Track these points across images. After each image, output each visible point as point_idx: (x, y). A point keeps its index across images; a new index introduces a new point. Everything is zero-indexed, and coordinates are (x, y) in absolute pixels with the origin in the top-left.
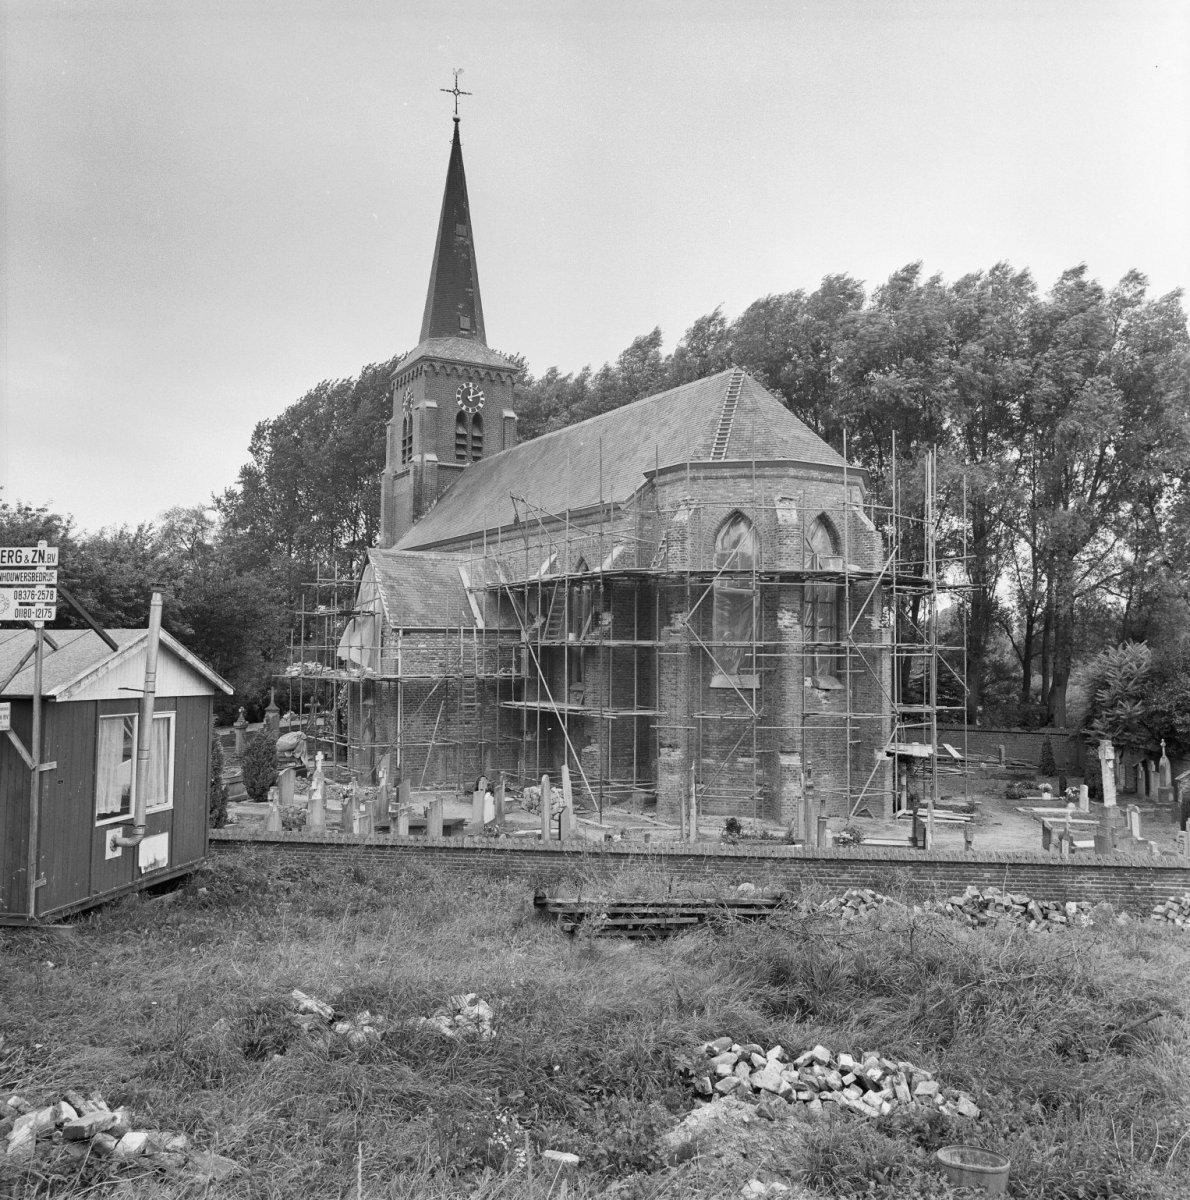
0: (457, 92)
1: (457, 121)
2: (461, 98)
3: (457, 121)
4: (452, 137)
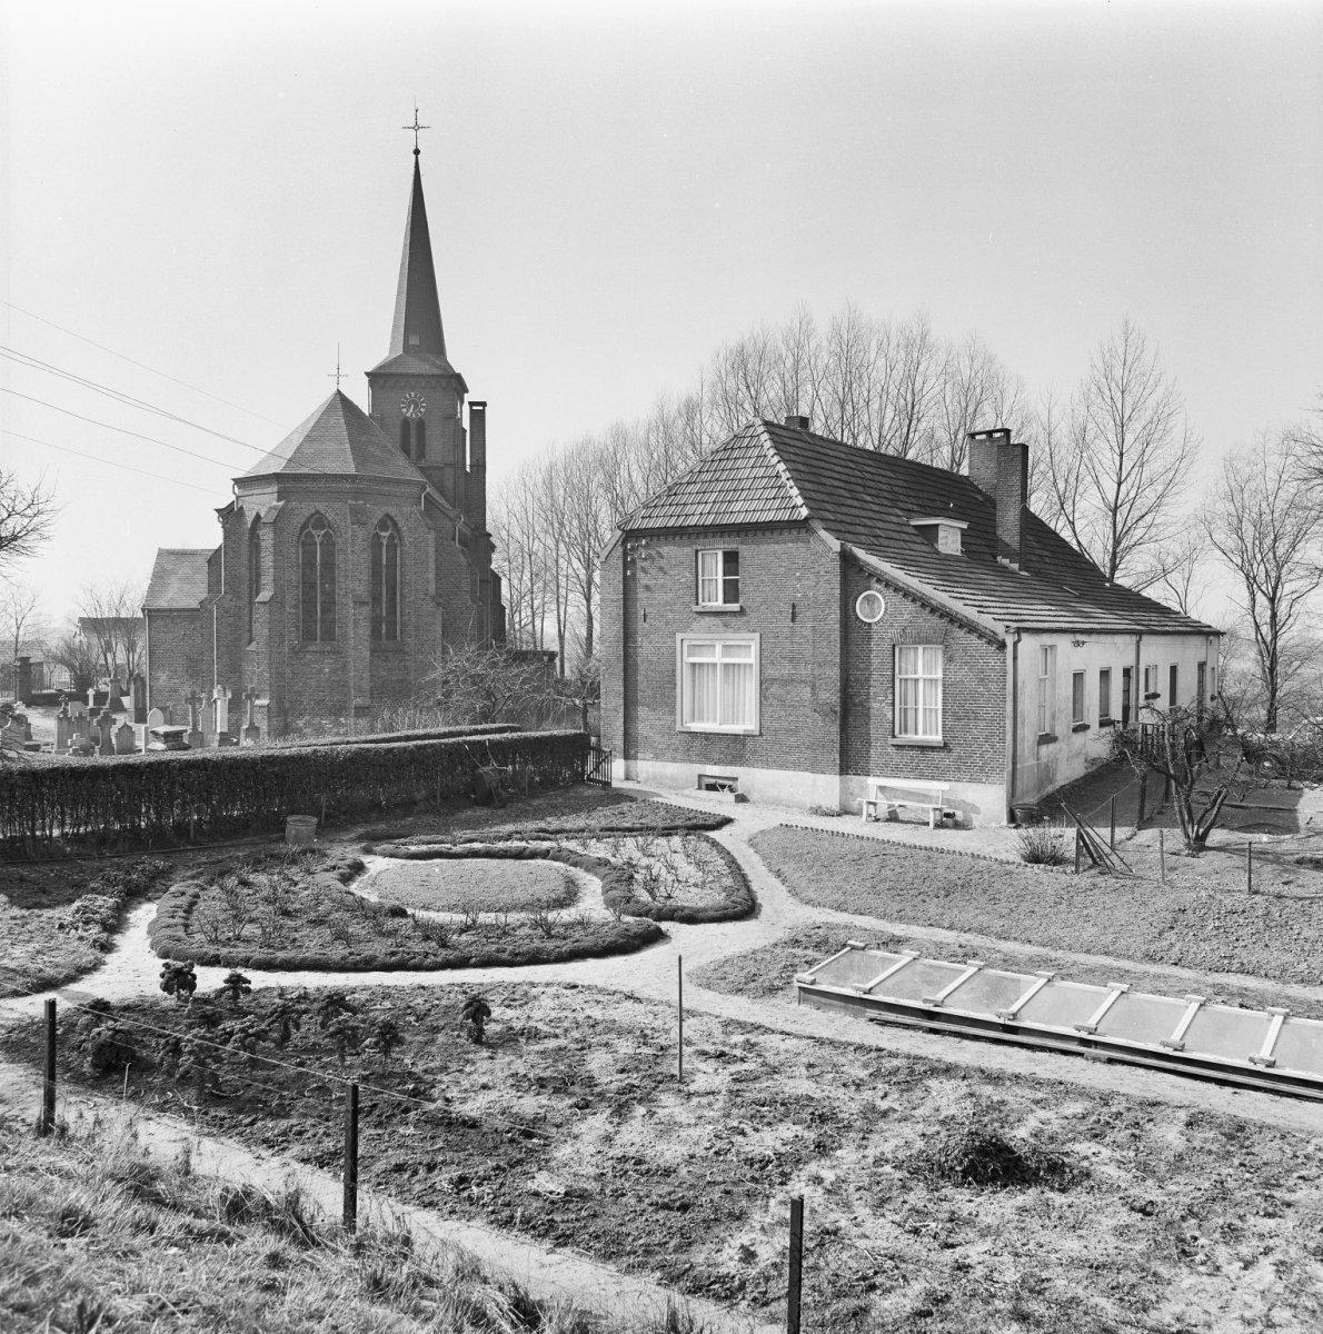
0: (416, 127)
1: (417, 152)
2: (420, 131)
3: (417, 152)
4: (412, 171)
